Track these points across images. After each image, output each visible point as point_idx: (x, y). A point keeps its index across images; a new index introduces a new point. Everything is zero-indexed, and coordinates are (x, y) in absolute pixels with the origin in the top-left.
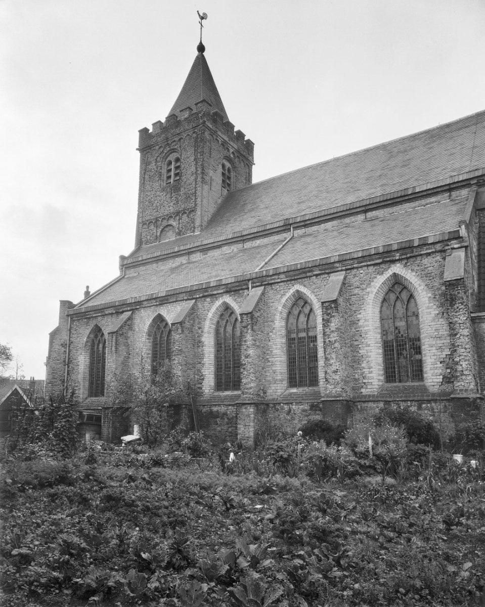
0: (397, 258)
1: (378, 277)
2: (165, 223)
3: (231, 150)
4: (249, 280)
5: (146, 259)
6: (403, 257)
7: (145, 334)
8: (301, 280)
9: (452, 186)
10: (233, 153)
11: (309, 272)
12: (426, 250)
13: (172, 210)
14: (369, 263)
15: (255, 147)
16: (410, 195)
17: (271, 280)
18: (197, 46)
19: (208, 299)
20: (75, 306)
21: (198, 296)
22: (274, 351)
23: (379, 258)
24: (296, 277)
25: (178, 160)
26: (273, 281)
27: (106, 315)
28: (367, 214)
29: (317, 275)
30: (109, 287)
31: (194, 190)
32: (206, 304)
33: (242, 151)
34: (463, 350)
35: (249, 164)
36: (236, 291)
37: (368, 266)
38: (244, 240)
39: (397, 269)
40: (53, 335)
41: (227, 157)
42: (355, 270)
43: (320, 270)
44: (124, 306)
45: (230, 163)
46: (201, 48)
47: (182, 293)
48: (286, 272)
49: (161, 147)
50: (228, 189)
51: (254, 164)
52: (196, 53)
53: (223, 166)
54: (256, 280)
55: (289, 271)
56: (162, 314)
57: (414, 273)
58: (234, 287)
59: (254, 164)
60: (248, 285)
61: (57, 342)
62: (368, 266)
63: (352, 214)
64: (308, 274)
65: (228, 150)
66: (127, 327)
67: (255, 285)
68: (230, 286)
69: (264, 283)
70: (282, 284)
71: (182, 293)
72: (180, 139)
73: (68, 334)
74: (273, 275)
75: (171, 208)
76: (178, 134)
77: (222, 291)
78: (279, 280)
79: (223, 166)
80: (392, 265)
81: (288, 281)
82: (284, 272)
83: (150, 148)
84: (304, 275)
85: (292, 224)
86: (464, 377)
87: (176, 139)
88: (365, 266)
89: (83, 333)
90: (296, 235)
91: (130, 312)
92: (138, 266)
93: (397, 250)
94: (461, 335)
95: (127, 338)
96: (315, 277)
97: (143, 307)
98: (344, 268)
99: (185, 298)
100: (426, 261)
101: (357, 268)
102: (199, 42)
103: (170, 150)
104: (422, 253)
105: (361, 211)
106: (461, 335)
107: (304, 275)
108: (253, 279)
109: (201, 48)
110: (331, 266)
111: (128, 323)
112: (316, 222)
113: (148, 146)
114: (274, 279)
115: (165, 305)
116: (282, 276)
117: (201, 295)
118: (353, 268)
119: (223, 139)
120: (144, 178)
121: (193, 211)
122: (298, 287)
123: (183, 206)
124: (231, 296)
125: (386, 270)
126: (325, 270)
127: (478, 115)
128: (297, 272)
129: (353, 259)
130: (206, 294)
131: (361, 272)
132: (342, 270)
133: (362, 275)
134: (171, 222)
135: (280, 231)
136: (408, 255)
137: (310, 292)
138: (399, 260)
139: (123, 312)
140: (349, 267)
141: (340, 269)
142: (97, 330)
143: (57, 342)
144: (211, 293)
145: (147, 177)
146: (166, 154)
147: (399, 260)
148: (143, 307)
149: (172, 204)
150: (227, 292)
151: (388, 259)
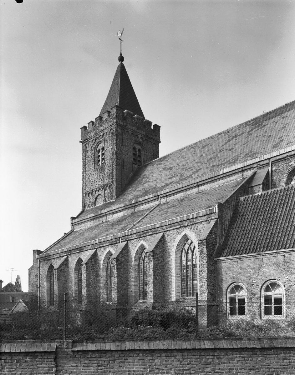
0: (187, 225)
1: (178, 236)
2: (97, 193)
3: (140, 136)
4: (120, 238)
5: (84, 219)
6: (190, 224)
7: (74, 270)
8: (143, 238)
9: (244, 169)
10: (141, 138)
11: (147, 233)
12: (200, 220)
13: (101, 184)
14: (174, 228)
15: (161, 128)
16: (221, 175)
17: (130, 238)
18: (118, 58)
19: (102, 249)
20: (42, 252)
21: (97, 247)
22: (132, 279)
23: (179, 225)
24: (141, 236)
25: (103, 149)
26: (131, 239)
27: (55, 258)
28: (113, 215)
29: (151, 235)
30: (64, 238)
31: (112, 171)
32: (101, 252)
33: (152, 134)
34: (204, 279)
35: (157, 142)
36: (114, 244)
37: (174, 229)
38: (134, 206)
39: (186, 231)
40: (30, 270)
41: (137, 142)
42: (168, 232)
43: (152, 232)
44: (63, 253)
45: (140, 146)
46: (121, 59)
47: (89, 245)
48: (137, 233)
49: (93, 140)
50: (139, 164)
51: (161, 142)
52: (119, 63)
53: (134, 149)
54: (123, 238)
55: (172, 224)
56: (81, 258)
57: (194, 234)
58: (113, 242)
59: (161, 142)
60: (119, 240)
61: (33, 274)
62: (174, 229)
63: (191, 188)
64: (147, 234)
65: (138, 137)
66: (64, 266)
67: (123, 240)
68: (111, 241)
69: (127, 239)
70: (135, 240)
71: (89, 245)
72: (104, 134)
73: (283, 258)
74: (130, 235)
75: (100, 183)
76: (102, 131)
77: (107, 244)
78: (134, 238)
79: (134, 149)
80: (185, 229)
81: (138, 238)
82: (135, 233)
83: (88, 141)
84: (144, 235)
85: (270, 158)
86: (204, 294)
87: (101, 134)
88: (172, 229)
89: (45, 268)
90: (162, 203)
91: (66, 257)
92: (145, 204)
93: (186, 220)
94: (204, 271)
95: (64, 272)
96: (150, 236)
97: (72, 254)
98: (163, 231)
99: (91, 248)
100: (200, 226)
101: (169, 230)
102: (120, 54)
103: (98, 142)
104: (198, 222)
105: (195, 186)
106: (204, 271)
107: (144, 235)
108: (121, 237)
109: (121, 59)
110: (157, 229)
111: (65, 263)
112: (210, 181)
113: (87, 140)
114: (131, 237)
115: (82, 252)
116: (135, 235)
117: (98, 247)
118: (167, 231)
119: (132, 130)
120: (85, 162)
121: (112, 185)
122: (142, 242)
123: (106, 182)
124: (112, 247)
125: (182, 232)
126: (154, 232)
127: (293, 102)
128: (142, 233)
129: (166, 225)
130: (100, 246)
131: (171, 233)
132: (162, 232)
133: (171, 235)
134: (100, 192)
135: (153, 200)
136: (192, 223)
137: (148, 245)
138: (188, 226)
139: (63, 256)
140: (165, 230)
141: (161, 231)
142: (51, 267)
143: (33, 274)
144: (103, 245)
145: (87, 161)
146: (97, 144)
147: (188, 226)
148: (72, 254)
149: (100, 180)
150: (110, 245)
151: (183, 226)
